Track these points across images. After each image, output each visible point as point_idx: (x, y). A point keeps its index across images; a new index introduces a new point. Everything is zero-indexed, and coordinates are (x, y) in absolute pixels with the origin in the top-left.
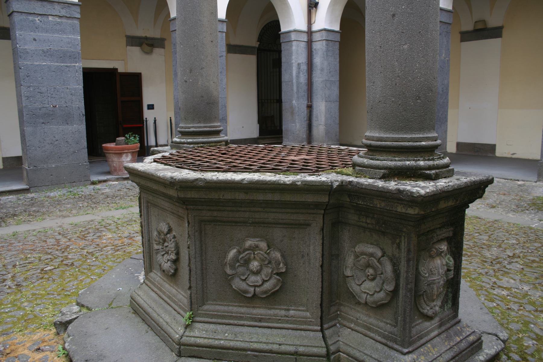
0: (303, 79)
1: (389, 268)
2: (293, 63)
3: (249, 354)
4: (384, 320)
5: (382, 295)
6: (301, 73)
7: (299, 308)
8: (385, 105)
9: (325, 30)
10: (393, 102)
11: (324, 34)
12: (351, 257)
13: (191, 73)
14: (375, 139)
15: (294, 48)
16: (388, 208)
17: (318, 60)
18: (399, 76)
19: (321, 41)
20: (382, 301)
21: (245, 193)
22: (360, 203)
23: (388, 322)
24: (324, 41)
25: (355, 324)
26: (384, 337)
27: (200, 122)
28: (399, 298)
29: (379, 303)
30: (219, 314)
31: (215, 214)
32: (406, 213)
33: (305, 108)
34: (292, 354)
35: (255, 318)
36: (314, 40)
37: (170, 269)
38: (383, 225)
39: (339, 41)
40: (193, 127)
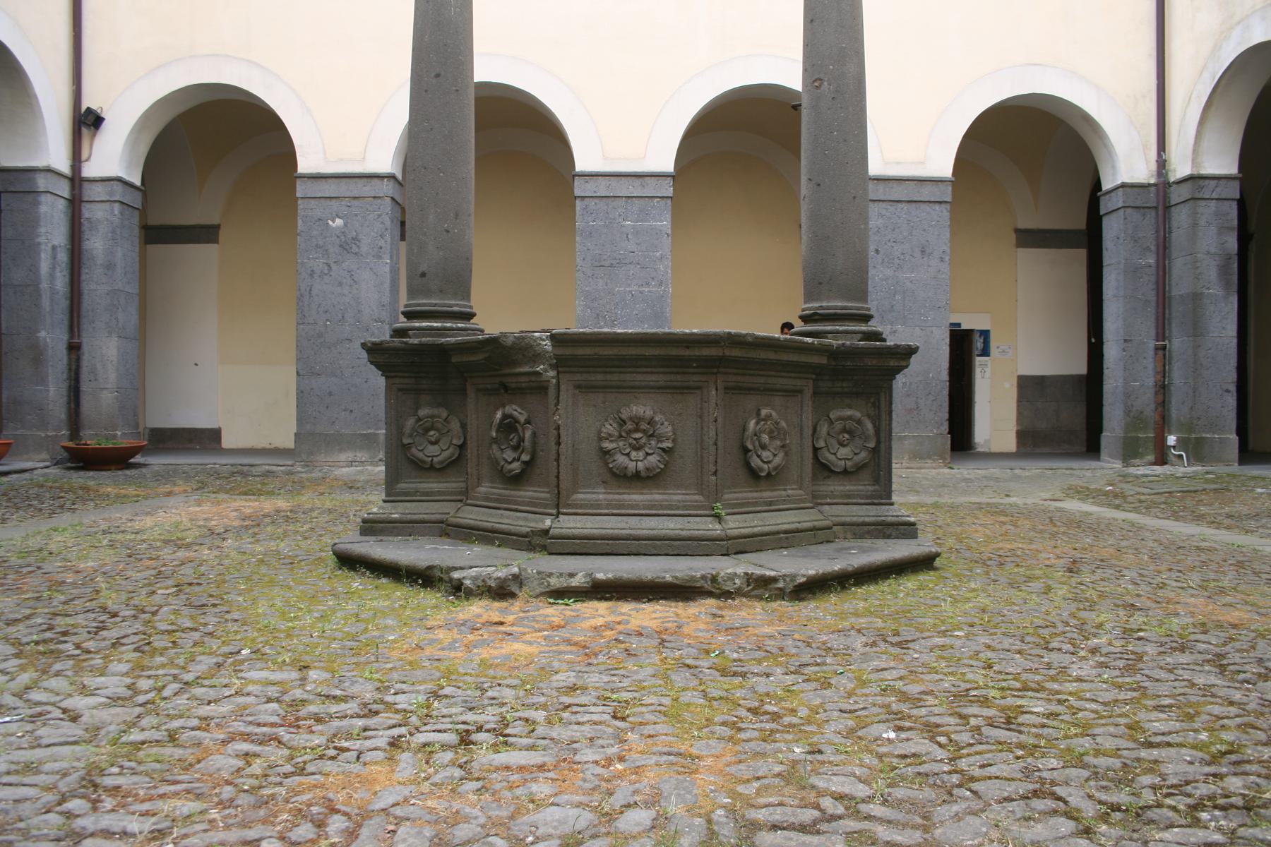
0: (61, 282)
1: (869, 426)
2: (39, 244)
5: (863, 455)
6: (58, 269)
9: (119, 180)
11: (119, 192)
13: (456, 218)
15: (43, 209)
17: (96, 245)
19: (108, 203)
21: (776, 352)
24: (117, 205)
26: (867, 497)
28: (342, 727)
33: (65, 352)
34: (811, 530)
35: (766, 502)
36: (85, 199)
37: (659, 464)
39: (1238, 197)
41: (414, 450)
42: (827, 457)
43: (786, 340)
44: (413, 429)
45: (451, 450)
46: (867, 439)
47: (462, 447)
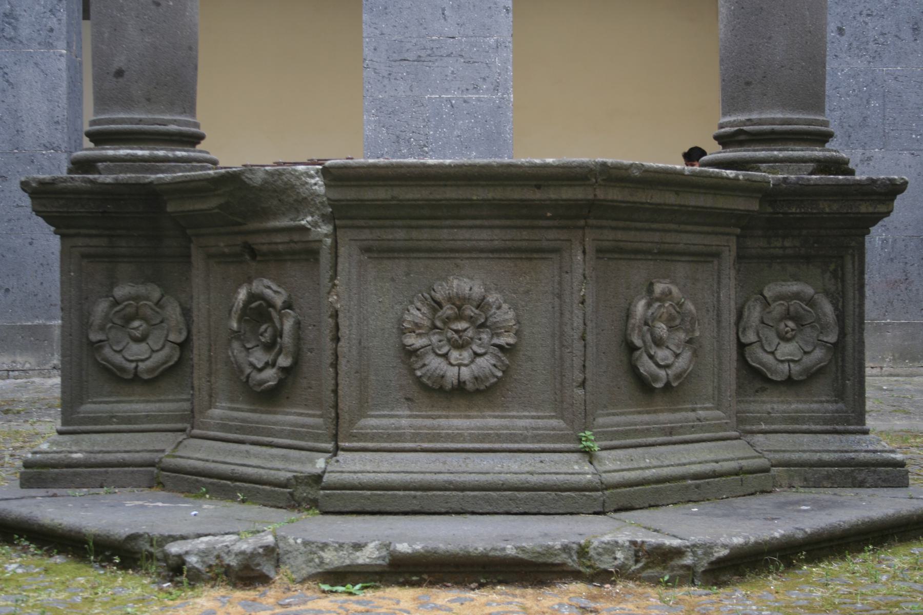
3: (690, 485)
4: (815, 399)
7: (705, 405)
8: (791, 72)
10: (802, 67)
12: (754, 308)
14: (778, 122)
16: (845, 211)
18: (810, 32)
20: (821, 362)
21: (677, 193)
22: (794, 210)
23: (824, 399)
25: (766, 423)
27: (185, 112)
29: (815, 369)
30: (621, 429)
31: (620, 235)
32: (875, 213)
35: (663, 429)
38: (816, 245)
40: (174, 122)
41: (107, 352)
42: (760, 357)
43: (694, 174)
44: (106, 318)
45: (166, 351)
46: (824, 329)
47: (184, 346)
